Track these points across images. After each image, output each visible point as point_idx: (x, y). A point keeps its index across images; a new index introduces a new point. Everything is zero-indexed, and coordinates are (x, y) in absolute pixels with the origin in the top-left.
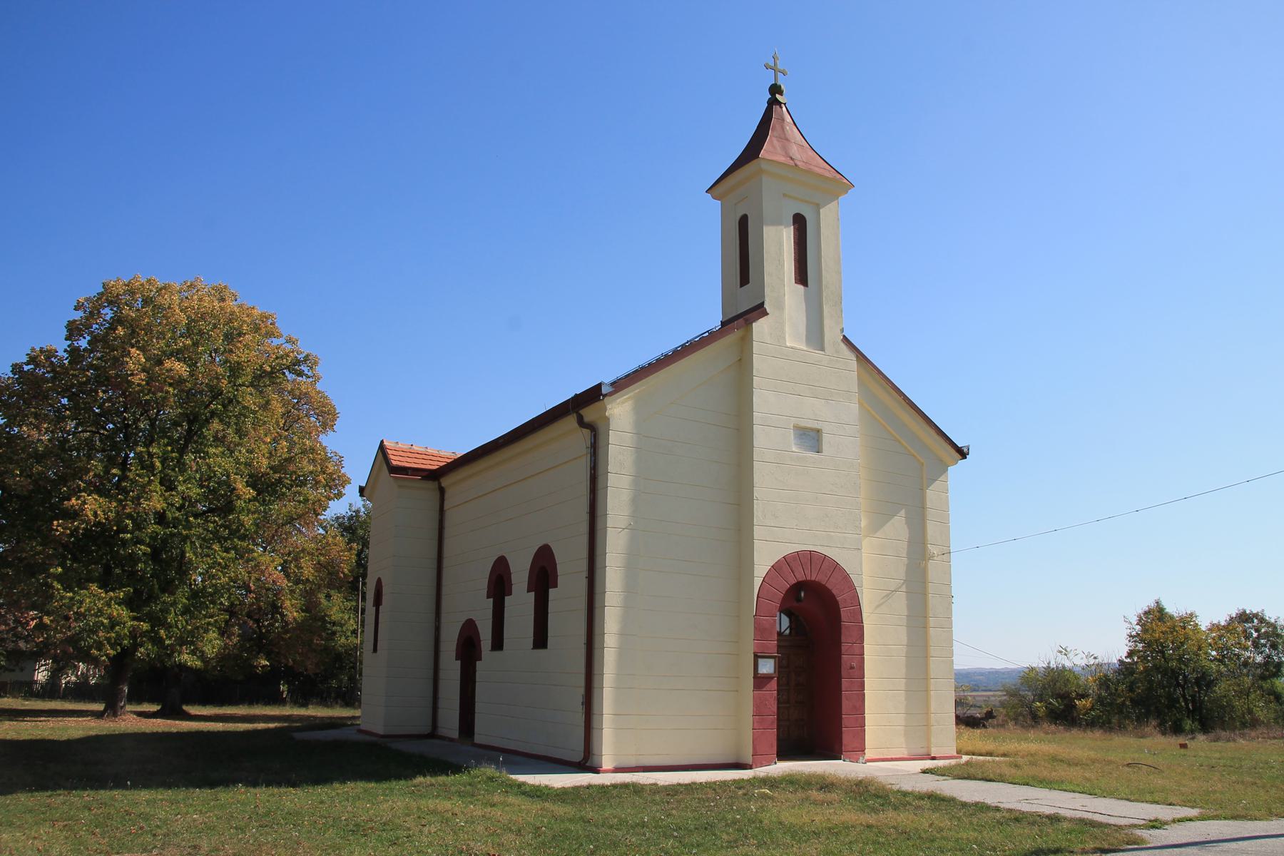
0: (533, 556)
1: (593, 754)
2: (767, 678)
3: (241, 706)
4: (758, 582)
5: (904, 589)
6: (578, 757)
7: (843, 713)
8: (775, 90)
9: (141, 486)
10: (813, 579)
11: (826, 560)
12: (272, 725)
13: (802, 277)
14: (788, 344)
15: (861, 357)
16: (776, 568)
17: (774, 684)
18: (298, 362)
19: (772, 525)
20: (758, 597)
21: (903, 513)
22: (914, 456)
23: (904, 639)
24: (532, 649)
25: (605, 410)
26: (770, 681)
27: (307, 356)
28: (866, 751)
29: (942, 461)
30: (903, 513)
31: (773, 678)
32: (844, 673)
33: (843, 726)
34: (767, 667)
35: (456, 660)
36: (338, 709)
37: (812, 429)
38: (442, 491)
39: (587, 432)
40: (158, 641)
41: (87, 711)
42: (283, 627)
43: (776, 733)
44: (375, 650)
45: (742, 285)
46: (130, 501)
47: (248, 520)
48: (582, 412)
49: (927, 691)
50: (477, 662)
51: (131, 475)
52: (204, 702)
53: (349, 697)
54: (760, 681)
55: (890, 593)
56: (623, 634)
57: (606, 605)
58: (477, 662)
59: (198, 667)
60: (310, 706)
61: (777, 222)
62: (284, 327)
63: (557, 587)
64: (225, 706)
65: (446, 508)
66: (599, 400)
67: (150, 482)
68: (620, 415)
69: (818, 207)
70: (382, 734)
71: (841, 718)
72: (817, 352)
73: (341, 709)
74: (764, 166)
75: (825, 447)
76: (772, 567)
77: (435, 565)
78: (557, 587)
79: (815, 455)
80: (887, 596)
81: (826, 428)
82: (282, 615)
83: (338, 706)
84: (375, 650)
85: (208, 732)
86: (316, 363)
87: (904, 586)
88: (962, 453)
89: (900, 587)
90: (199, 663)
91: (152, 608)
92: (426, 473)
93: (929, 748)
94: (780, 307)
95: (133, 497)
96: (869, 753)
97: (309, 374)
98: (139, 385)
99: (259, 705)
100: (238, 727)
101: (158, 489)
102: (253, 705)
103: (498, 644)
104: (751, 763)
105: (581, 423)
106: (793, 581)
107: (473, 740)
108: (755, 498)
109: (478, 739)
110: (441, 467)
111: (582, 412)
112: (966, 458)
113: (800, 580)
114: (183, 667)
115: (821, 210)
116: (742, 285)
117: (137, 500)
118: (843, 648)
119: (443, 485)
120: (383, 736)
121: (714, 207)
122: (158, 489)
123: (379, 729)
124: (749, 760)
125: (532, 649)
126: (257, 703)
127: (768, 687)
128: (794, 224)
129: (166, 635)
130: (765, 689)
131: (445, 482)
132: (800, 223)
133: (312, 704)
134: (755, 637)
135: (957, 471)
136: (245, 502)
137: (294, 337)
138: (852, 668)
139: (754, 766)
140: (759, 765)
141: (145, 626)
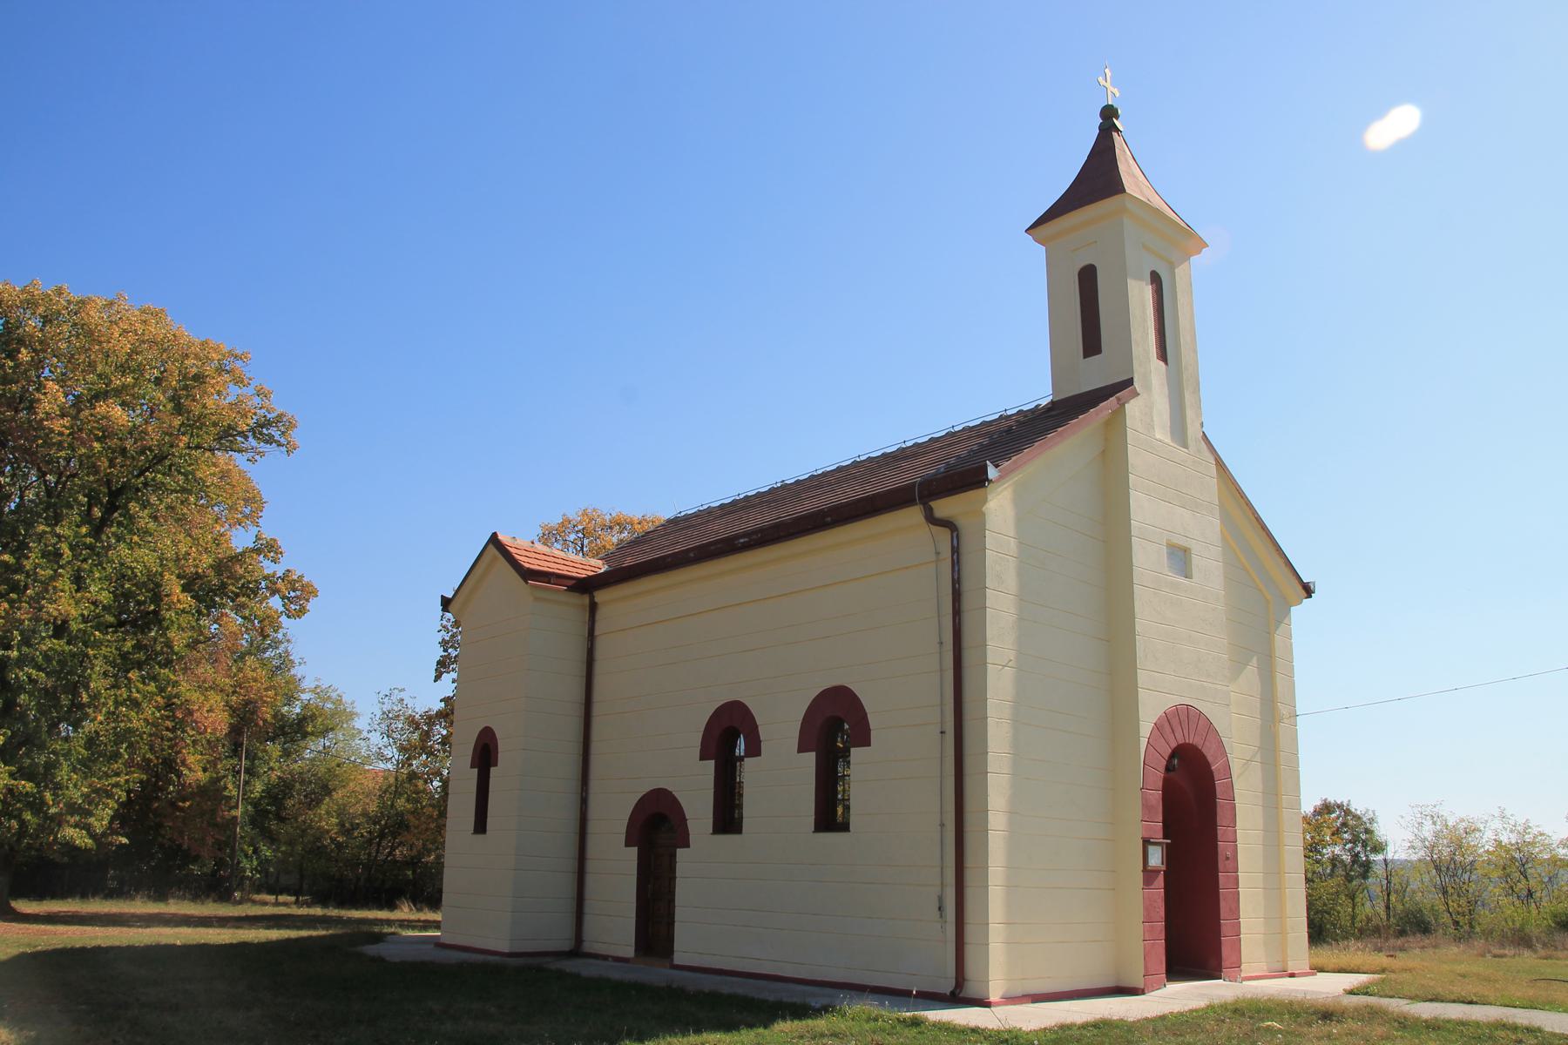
0: (810, 701)
1: (967, 980)
2: (1156, 872)
3: (70, 900)
5: (1258, 758)
6: (947, 987)
7: (1222, 918)
8: (1109, 114)
9: (41, 582)
10: (1191, 742)
11: (1191, 713)
12: (275, 934)
13: (1163, 355)
14: (1158, 436)
15: (1220, 464)
16: (1158, 726)
17: (1161, 877)
18: (267, 423)
20: (1144, 764)
21: (1255, 659)
22: (1260, 590)
24: (814, 832)
25: (985, 501)
27: (281, 416)
28: (1242, 967)
31: (1159, 871)
32: (1221, 866)
34: (1156, 858)
35: (627, 845)
36: (211, 904)
38: (593, 608)
39: (944, 535)
40: (37, 806)
41: (133, 916)
42: (178, 792)
43: (1164, 945)
44: (480, 826)
45: (1086, 355)
46: (26, 602)
47: (179, 639)
48: (933, 504)
50: (679, 851)
51: (28, 565)
52: (40, 896)
53: (427, 892)
54: (1149, 874)
56: (1012, 813)
57: (989, 770)
58: (679, 851)
59: (89, 846)
60: (171, 901)
61: (1139, 278)
62: (257, 371)
63: (869, 745)
64: (45, 899)
65: (596, 633)
66: (984, 486)
67: (53, 578)
70: (507, 951)
71: (1219, 925)
73: (215, 905)
75: (1195, 572)
76: (1155, 724)
77: (580, 710)
78: (869, 745)
79: (1182, 580)
80: (1245, 764)
81: (1195, 548)
82: (179, 775)
83: (211, 900)
84: (480, 826)
85: (129, 947)
86: (291, 425)
87: (1259, 755)
88: (1308, 590)
90: (89, 841)
91: (33, 759)
92: (574, 582)
93: (1284, 961)
94: (1148, 388)
95: (31, 598)
96: (1247, 970)
97: (282, 440)
98: (60, 434)
99: (97, 899)
100: (160, 935)
101: (67, 588)
102: (88, 898)
103: (728, 818)
104: (1142, 987)
105: (931, 519)
106: (1174, 745)
107: (672, 960)
109: (679, 958)
110: (589, 577)
111: (933, 504)
112: (1311, 597)
113: (1180, 742)
114: (70, 848)
115: (1176, 271)
116: (1086, 355)
117: (35, 602)
118: (1218, 832)
119: (596, 600)
120: (510, 955)
121: (1035, 255)
122: (67, 588)
123: (504, 946)
124: (1140, 984)
125: (814, 832)
126: (94, 896)
128: (1152, 284)
129: (53, 800)
130: (1153, 887)
131: (601, 596)
132: (1156, 279)
133: (174, 898)
134: (1143, 815)
135: (1302, 614)
136: (177, 614)
137: (267, 387)
138: (1227, 858)
139: (1146, 991)
140: (1150, 989)
141: (28, 786)
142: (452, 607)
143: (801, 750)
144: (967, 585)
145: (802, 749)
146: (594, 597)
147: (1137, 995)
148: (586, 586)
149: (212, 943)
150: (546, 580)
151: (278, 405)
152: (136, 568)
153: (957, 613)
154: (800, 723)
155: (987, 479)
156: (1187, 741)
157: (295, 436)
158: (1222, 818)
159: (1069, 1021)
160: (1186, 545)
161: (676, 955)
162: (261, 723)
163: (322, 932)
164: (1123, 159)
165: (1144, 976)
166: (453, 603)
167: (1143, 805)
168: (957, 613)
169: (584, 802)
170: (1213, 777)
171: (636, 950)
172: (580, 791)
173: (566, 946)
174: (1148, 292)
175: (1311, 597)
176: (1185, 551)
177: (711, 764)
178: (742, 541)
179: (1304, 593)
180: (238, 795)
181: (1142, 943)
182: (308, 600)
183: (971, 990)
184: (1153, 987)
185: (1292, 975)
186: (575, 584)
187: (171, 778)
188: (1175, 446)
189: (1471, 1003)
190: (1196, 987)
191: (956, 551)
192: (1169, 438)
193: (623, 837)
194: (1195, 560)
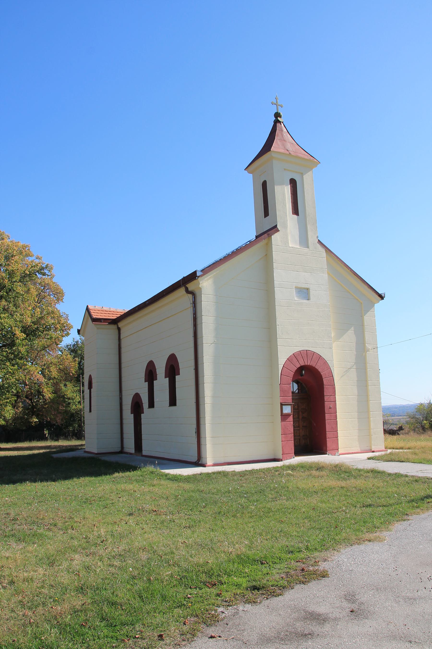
2: (288, 415)
4: (281, 367)
5: (355, 367)
10: (308, 364)
12: (41, 451)
14: (290, 246)
16: (289, 360)
17: (291, 418)
18: (43, 269)
19: (287, 338)
21: (353, 328)
22: (357, 299)
23: (356, 392)
26: (289, 417)
27: (47, 265)
28: (339, 449)
29: (371, 301)
30: (353, 328)
31: (291, 415)
32: (326, 411)
33: (327, 438)
34: (287, 410)
37: (304, 288)
38: (119, 329)
39: (190, 296)
44: (90, 411)
45: (265, 217)
48: (187, 286)
49: (369, 418)
54: (284, 417)
55: (348, 370)
56: (214, 397)
61: (282, 184)
62: (35, 251)
65: (121, 338)
68: (207, 286)
69: (302, 174)
71: (326, 434)
72: (305, 249)
74: (273, 155)
75: (311, 297)
80: (347, 370)
84: (90, 411)
85: (10, 456)
88: (382, 297)
89: (353, 366)
93: (371, 446)
94: (285, 227)
96: (341, 451)
103: (151, 405)
105: (187, 291)
106: (298, 366)
107: (142, 453)
108: (277, 325)
109: (144, 453)
110: (118, 317)
111: (187, 286)
112: (383, 299)
113: (302, 365)
116: (265, 217)
119: (119, 326)
124: (280, 457)
127: (288, 420)
131: (120, 325)
132: (293, 182)
135: (380, 305)
136: (21, 340)
137: (40, 256)
138: (330, 408)
139: (283, 460)
142: (81, 332)
143: (165, 378)
144: (198, 315)
145: (166, 377)
146: (118, 325)
147: (279, 461)
148: (114, 322)
149: (3, 456)
150: (100, 321)
151: (45, 261)
152: (6, 326)
153: (195, 325)
154: (165, 367)
155: (197, 276)
156: (306, 364)
157: (53, 272)
158: (327, 392)
159: (195, 473)
160: (308, 287)
161: (143, 451)
162: (71, 374)
163: (48, 450)
164: (280, 134)
165: (282, 454)
166: (81, 330)
167: (280, 390)
168: (195, 325)
169: (121, 399)
170: (322, 377)
171: (135, 450)
172: (119, 395)
173: (119, 450)
174: (287, 190)
175: (383, 299)
176: (308, 289)
177: (147, 383)
178: (147, 303)
179: (379, 298)
180: (81, 400)
181: (281, 442)
182: (70, 330)
183: (202, 461)
184: (287, 458)
185: (373, 452)
186: (111, 321)
187: (40, 397)
188: (303, 248)
189: (402, 462)
190: (320, 457)
191: (194, 303)
192: (299, 246)
193: (130, 411)
194: (312, 293)
